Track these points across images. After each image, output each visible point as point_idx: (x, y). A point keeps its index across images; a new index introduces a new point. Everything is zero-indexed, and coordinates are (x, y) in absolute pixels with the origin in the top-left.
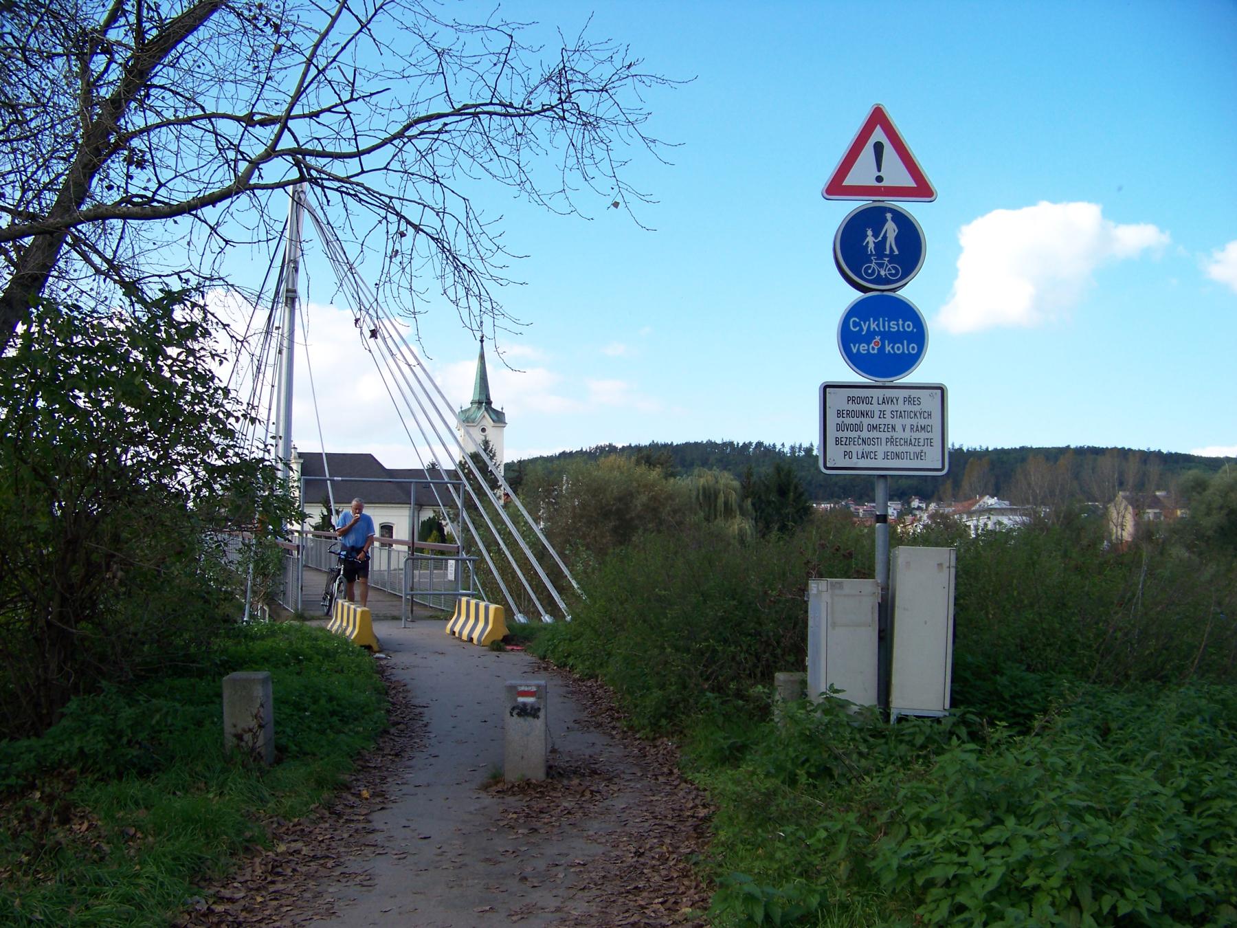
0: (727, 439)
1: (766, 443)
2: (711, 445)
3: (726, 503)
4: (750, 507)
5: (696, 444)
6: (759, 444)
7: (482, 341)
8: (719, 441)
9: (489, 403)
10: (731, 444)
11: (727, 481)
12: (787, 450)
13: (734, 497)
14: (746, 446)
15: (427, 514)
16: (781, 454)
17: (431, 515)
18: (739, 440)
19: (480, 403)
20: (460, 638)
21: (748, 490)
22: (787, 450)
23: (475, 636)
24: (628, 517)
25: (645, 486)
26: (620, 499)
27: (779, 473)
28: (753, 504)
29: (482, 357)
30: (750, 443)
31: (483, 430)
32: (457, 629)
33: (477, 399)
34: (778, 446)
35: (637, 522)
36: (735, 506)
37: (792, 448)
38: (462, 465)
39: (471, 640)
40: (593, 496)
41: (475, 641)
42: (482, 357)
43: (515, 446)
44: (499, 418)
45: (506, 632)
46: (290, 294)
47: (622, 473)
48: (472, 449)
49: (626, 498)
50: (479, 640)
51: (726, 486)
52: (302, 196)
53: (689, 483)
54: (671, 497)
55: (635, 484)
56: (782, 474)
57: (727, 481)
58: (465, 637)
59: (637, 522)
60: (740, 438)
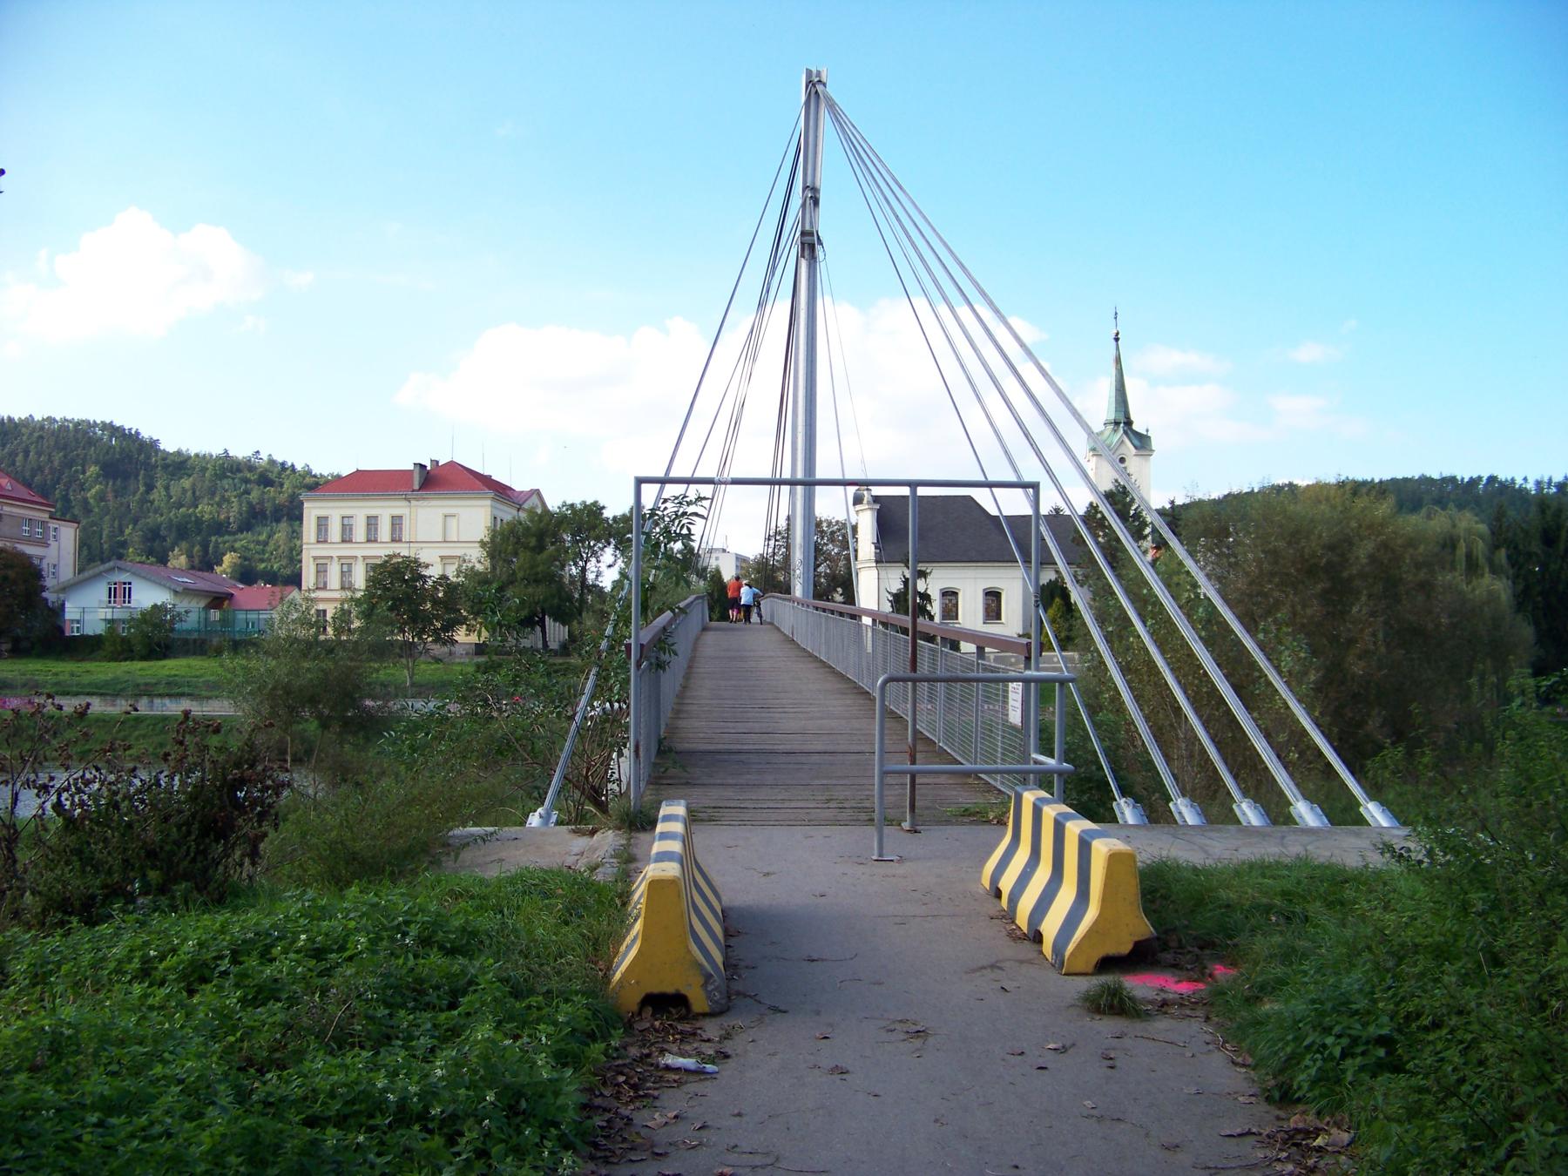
0: (1447, 473)
1: (1502, 477)
2: (1425, 481)
3: (1469, 556)
4: (1504, 561)
5: (1405, 480)
6: (1492, 479)
7: (1117, 340)
8: (1436, 476)
9: (1129, 423)
10: (1453, 479)
11: (1470, 524)
12: (1531, 486)
13: (1480, 548)
14: (1474, 482)
15: (1048, 576)
16: (1522, 492)
17: (1053, 576)
18: (1464, 473)
19: (1117, 423)
20: (1010, 916)
21: (1500, 536)
22: (1531, 486)
23: (1050, 927)
24: (1345, 574)
25: (1370, 527)
26: (1331, 548)
27: (1543, 512)
28: (1509, 557)
29: (1118, 360)
30: (1480, 478)
31: (1122, 460)
32: (1006, 884)
33: (1112, 417)
34: (1519, 481)
35: (1357, 583)
36: (1482, 560)
37: (1538, 483)
38: (1093, 508)
39: (1037, 938)
40: (1289, 543)
41: (1047, 947)
42: (1118, 360)
43: (1160, 488)
44: (1142, 442)
45: (1143, 928)
46: (807, 238)
47: (1334, 507)
48: (1106, 485)
49: (1341, 546)
50: (1058, 948)
51: (1469, 531)
52: (820, 88)
53: (1439, 523)
54: (1411, 543)
55: (1354, 524)
56: (1549, 513)
57: (1470, 524)
58: (1022, 920)
59: (1357, 583)
60: (1464, 471)
